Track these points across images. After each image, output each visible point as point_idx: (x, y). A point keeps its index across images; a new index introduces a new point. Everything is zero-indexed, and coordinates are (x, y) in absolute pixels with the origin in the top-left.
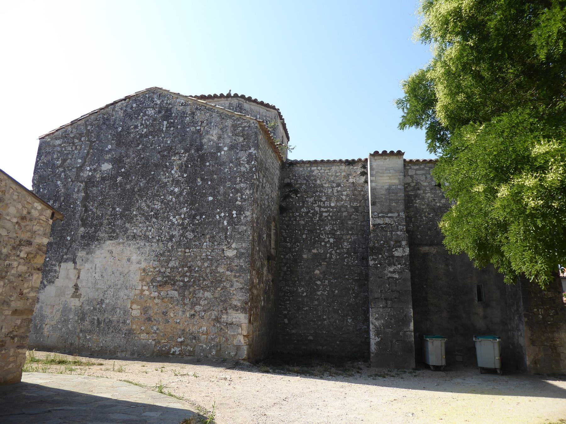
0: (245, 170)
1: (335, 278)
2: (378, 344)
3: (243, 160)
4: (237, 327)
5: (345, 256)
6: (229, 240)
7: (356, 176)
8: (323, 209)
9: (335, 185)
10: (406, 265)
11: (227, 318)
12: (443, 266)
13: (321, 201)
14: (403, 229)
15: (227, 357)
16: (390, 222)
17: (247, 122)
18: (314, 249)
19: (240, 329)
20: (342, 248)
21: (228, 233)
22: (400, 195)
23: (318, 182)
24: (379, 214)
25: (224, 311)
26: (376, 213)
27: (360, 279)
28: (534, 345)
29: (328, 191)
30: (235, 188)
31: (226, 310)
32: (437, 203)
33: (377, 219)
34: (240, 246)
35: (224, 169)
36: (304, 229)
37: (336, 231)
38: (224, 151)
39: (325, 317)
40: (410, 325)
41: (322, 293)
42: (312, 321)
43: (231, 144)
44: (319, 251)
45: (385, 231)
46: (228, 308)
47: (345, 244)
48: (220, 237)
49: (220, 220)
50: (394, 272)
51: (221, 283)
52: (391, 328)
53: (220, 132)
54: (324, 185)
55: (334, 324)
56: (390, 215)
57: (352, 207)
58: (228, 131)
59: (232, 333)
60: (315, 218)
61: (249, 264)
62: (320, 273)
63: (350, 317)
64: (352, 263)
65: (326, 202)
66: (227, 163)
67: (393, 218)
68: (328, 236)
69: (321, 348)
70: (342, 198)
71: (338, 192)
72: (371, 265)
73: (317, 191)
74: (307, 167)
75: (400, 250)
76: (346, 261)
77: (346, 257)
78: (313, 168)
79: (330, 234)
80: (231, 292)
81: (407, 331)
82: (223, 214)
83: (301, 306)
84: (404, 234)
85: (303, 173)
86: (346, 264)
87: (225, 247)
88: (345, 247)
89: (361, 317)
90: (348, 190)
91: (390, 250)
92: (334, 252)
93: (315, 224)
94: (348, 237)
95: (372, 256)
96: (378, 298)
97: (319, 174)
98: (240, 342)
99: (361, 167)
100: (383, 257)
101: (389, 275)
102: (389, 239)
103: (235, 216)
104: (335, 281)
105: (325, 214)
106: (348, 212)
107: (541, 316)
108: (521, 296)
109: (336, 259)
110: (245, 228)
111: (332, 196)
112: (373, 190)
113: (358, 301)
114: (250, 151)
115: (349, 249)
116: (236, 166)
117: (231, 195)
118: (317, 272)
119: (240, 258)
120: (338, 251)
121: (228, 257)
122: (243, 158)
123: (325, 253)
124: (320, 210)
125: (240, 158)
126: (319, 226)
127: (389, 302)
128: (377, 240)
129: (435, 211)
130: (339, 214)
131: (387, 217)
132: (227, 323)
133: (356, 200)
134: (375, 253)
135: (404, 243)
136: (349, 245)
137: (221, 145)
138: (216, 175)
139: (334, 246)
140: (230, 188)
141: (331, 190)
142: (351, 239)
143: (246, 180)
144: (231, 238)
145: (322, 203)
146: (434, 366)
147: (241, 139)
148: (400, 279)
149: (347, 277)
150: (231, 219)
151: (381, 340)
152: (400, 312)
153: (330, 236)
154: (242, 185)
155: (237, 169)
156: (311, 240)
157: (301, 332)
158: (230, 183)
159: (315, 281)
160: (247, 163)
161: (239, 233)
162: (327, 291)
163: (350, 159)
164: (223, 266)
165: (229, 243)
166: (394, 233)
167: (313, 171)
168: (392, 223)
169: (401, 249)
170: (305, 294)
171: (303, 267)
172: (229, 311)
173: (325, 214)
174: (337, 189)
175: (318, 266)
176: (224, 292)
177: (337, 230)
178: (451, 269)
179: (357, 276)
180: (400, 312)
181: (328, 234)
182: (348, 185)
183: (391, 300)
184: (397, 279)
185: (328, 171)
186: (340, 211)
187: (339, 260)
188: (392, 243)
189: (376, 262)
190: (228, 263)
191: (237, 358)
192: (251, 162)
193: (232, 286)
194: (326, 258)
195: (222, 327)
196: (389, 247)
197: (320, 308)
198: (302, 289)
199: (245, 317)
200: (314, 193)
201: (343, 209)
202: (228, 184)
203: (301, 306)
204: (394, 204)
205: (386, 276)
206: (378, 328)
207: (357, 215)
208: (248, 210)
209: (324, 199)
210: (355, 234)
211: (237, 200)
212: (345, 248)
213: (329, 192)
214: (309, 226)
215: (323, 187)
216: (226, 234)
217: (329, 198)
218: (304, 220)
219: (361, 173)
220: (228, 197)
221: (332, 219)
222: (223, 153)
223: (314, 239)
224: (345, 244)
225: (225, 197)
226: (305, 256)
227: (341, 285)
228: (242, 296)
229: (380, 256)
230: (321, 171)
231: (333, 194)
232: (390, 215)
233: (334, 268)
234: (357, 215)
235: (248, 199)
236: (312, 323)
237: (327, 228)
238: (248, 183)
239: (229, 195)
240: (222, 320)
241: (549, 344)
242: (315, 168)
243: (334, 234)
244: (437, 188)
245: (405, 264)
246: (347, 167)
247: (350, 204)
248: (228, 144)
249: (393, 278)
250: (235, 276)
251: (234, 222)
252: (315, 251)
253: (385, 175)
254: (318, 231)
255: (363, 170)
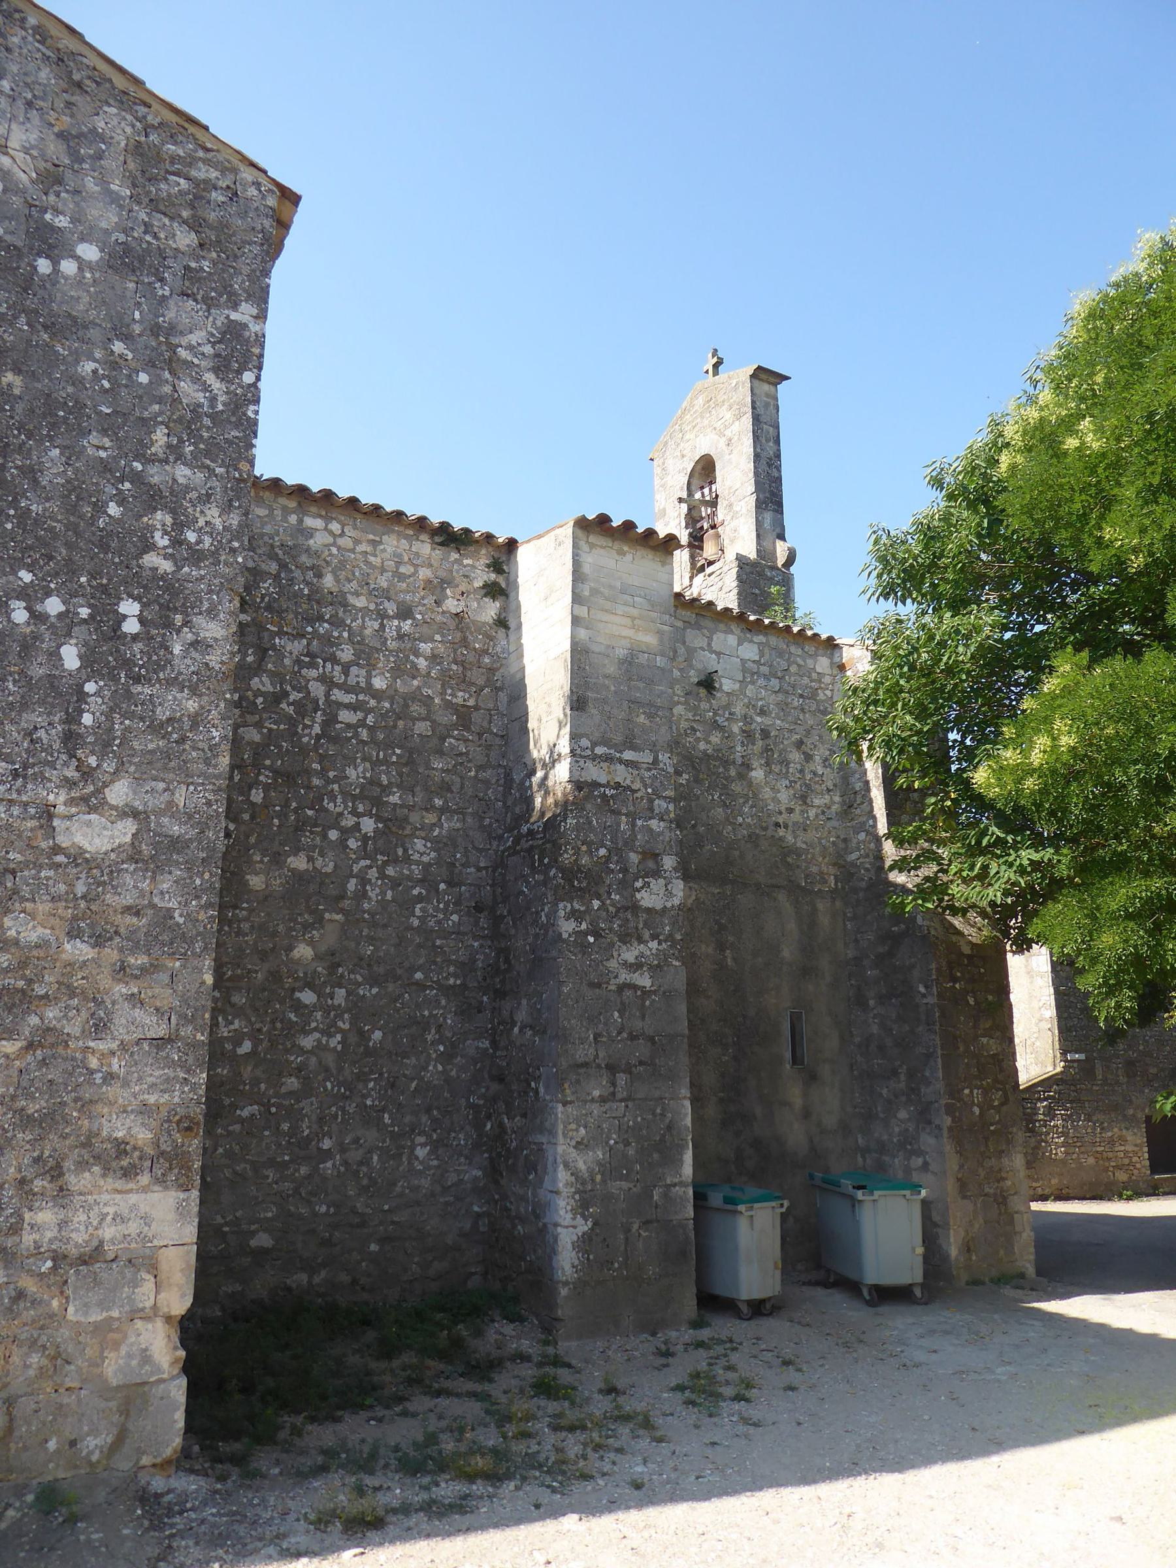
0: (201, 397)
1: (373, 981)
2: (585, 1243)
3: (190, 348)
4: (128, 1273)
5: (415, 892)
6: (93, 761)
7: (469, 593)
8: (338, 695)
9: (391, 608)
10: (674, 943)
11: (63, 1224)
12: (710, 950)
13: (334, 660)
14: (667, 811)
15: (56, 1472)
16: (628, 782)
17: (224, 171)
18: (296, 851)
19: (149, 1285)
20: (407, 859)
21: (87, 719)
22: (662, 692)
23: (328, 581)
24: (594, 744)
25: (38, 1184)
26: (585, 742)
27: (464, 986)
28: (964, 1197)
29: (363, 627)
30: (137, 479)
31: (56, 1172)
32: (698, 740)
33: (589, 764)
34: (161, 801)
35: (77, 358)
36: (257, 766)
37: (386, 790)
38: (77, 258)
39: (327, 1144)
40: (681, 1161)
41: (319, 1041)
42: (271, 1163)
43: (122, 238)
44: (319, 863)
45: (613, 812)
46: (68, 1164)
47: (419, 844)
48: (29, 734)
49: (36, 637)
50: (636, 967)
51: (27, 1012)
52: (626, 1178)
53: (55, 150)
54: (352, 600)
55: (365, 1169)
56: (628, 755)
57: (448, 705)
58: (111, 163)
59: (96, 1316)
60: (305, 727)
61: (209, 905)
62: (318, 957)
63: (422, 1139)
64: (439, 922)
65: (354, 670)
66: (94, 334)
67: (638, 769)
68: (354, 808)
69: (303, 1277)
70: (414, 666)
71: (401, 637)
72: (565, 936)
73: (321, 618)
74: (286, 511)
75: (657, 885)
76: (418, 912)
77: (420, 899)
78: (309, 522)
79: (362, 797)
80: (94, 1063)
81: (675, 1185)
82: (53, 606)
83: (227, 1102)
84: (671, 829)
85: (268, 529)
86: (416, 923)
87: (59, 798)
88: (416, 857)
89: (461, 1136)
90: (438, 637)
91: (626, 886)
92: (373, 874)
93: (304, 751)
94: (430, 818)
95: (571, 900)
96: (585, 1065)
97: (334, 550)
98: (145, 1357)
99: (488, 566)
100: (603, 907)
101: (624, 976)
102: (626, 843)
103: (131, 626)
104: (375, 990)
105: (346, 716)
106: (433, 722)
107: (977, 1110)
108: (939, 1052)
109: (383, 903)
110: (192, 705)
111: (378, 650)
112: (580, 652)
113: (453, 1073)
114: (234, 316)
115: (430, 865)
116: (150, 365)
117: (113, 509)
118: (303, 951)
119: (158, 870)
120: (390, 871)
121: (77, 857)
122: (194, 338)
123: (342, 874)
124: (327, 695)
125: (172, 329)
126: (322, 759)
127: (622, 1079)
128: (589, 844)
129: (694, 768)
130: (401, 723)
131: (621, 761)
132: (58, 1258)
133: (464, 682)
134: (580, 889)
135: (669, 862)
136: (432, 849)
137: (62, 222)
138: (17, 371)
139: (377, 851)
140: (105, 467)
141: (376, 625)
142: (441, 827)
143: (207, 454)
144: (104, 746)
145: (338, 668)
146: (750, 1303)
147: (185, 239)
148: (655, 992)
149: (419, 975)
150: (106, 638)
151: (592, 1229)
152: (654, 1114)
153: (361, 809)
154: (182, 473)
155: (156, 381)
156: (286, 816)
157: (219, 1220)
158: (107, 442)
159: (293, 990)
160: (216, 370)
161: (157, 728)
162: (341, 1031)
163: (457, 525)
164: (43, 907)
165: (87, 774)
166: (639, 823)
167: (310, 533)
168: (635, 786)
169: (662, 881)
170: (246, 1047)
171: (246, 926)
172: (77, 1181)
173: (346, 716)
174: (399, 628)
175: (306, 927)
176: (43, 1063)
177: (390, 783)
178: (729, 961)
179: (456, 976)
180: (654, 1114)
181: (354, 798)
182: (439, 618)
183: (628, 1070)
184: (646, 993)
185: (369, 549)
186: (403, 714)
187: (393, 908)
188: (634, 858)
189: (584, 926)
190: (80, 889)
191: (123, 1464)
192: (239, 372)
193: (100, 1028)
194: (342, 897)
195: (29, 1284)
196: (625, 870)
197: (309, 1106)
198: (236, 1024)
199: (180, 1210)
200: (311, 621)
201: (416, 709)
202: (99, 447)
203: (227, 1102)
204: (642, 719)
205: (613, 981)
206: (584, 1183)
207: (466, 740)
208: (212, 613)
209: (346, 654)
210: (455, 812)
211: (148, 546)
212: (418, 863)
213: (368, 632)
214: (280, 755)
215: (345, 605)
216: (73, 718)
217: (366, 656)
218: (259, 725)
219: (485, 586)
220: (93, 520)
221: (373, 741)
222: (68, 267)
223: (296, 811)
224: (419, 844)
225: (73, 509)
226: (256, 882)
227: (397, 1010)
228: (167, 1085)
229: (596, 904)
230: (340, 541)
231: (384, 643)
232: (628, 755)
233: (371, 940)
234: (466, 740)
235: (215, 554)
236: (271, 1174)
237: (351, 773)
238: (219, 470)
239: (100, 508)
240: (28, 1239)
241: (992, 1191)
242: (318, 523)
243: (377, 802)
244: (703, 692)
245: (670, 937)
246: (438, 553)
247: (443, 693)
248: (106, 232)
249: (634, 987)
250: (122, 971)
251: (128, 663)
252: (299, 863)
253: (620, 609)
254: (316, 782)
255: (493, 576)
